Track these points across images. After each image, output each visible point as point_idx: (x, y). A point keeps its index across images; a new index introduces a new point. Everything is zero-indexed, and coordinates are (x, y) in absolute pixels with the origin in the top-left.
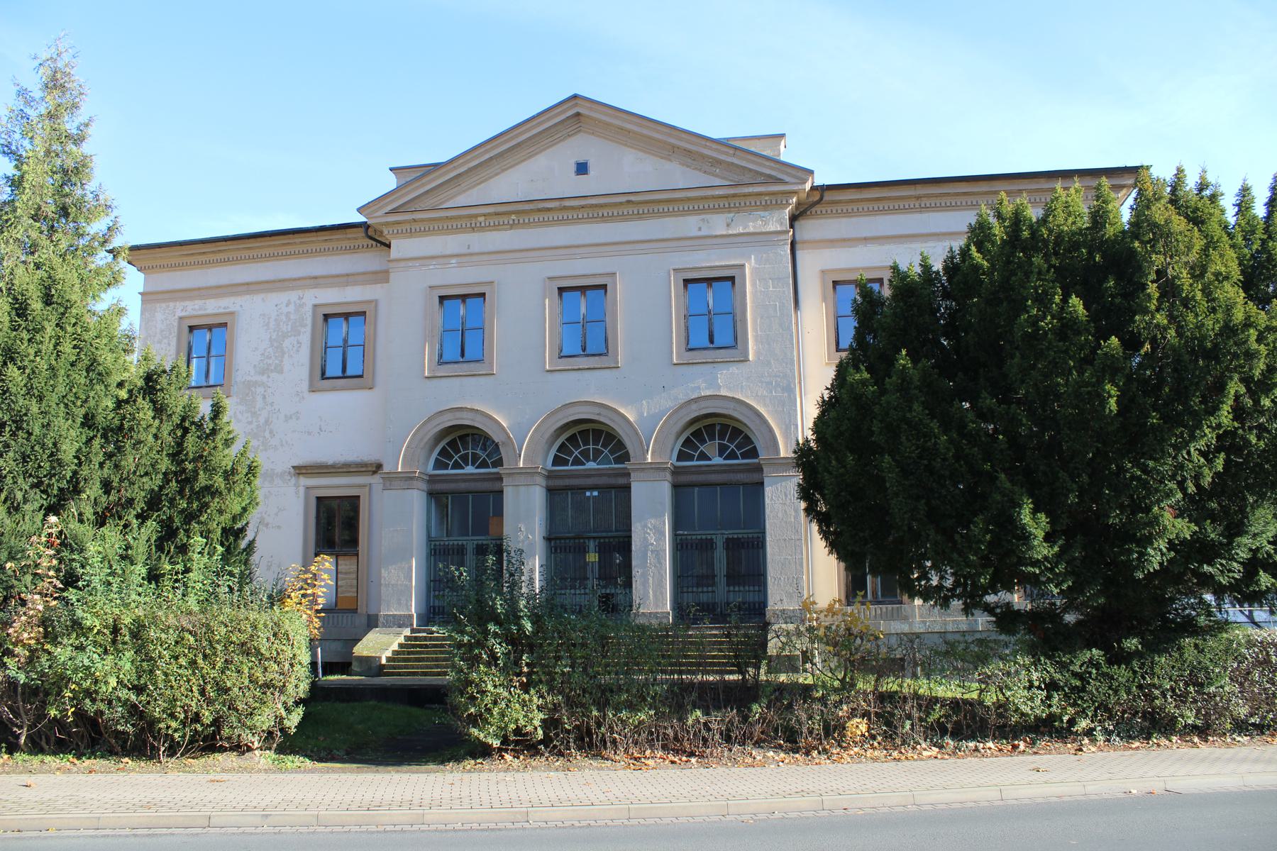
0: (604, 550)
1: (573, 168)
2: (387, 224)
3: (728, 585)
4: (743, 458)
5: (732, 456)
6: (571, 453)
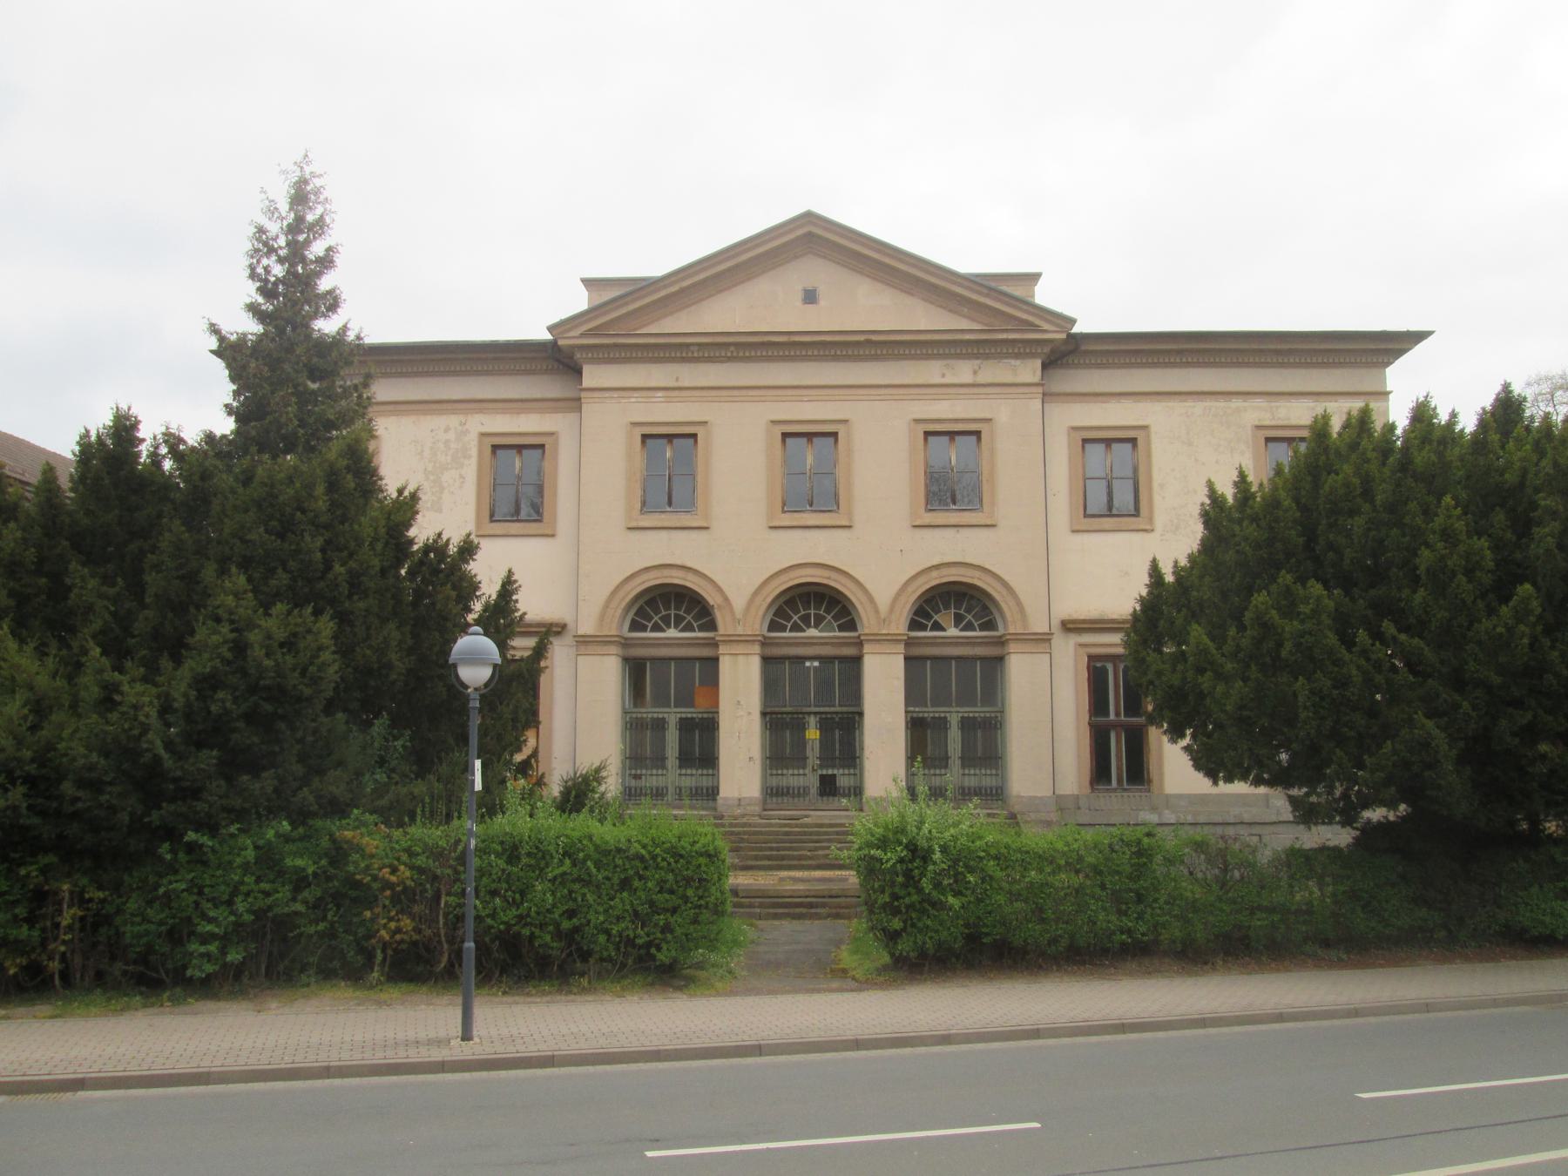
0: (826, 725)
1: (800, 296)
3: (963, 766)
4: (981, 629)
5: (969, 627)
6: (789, 618)
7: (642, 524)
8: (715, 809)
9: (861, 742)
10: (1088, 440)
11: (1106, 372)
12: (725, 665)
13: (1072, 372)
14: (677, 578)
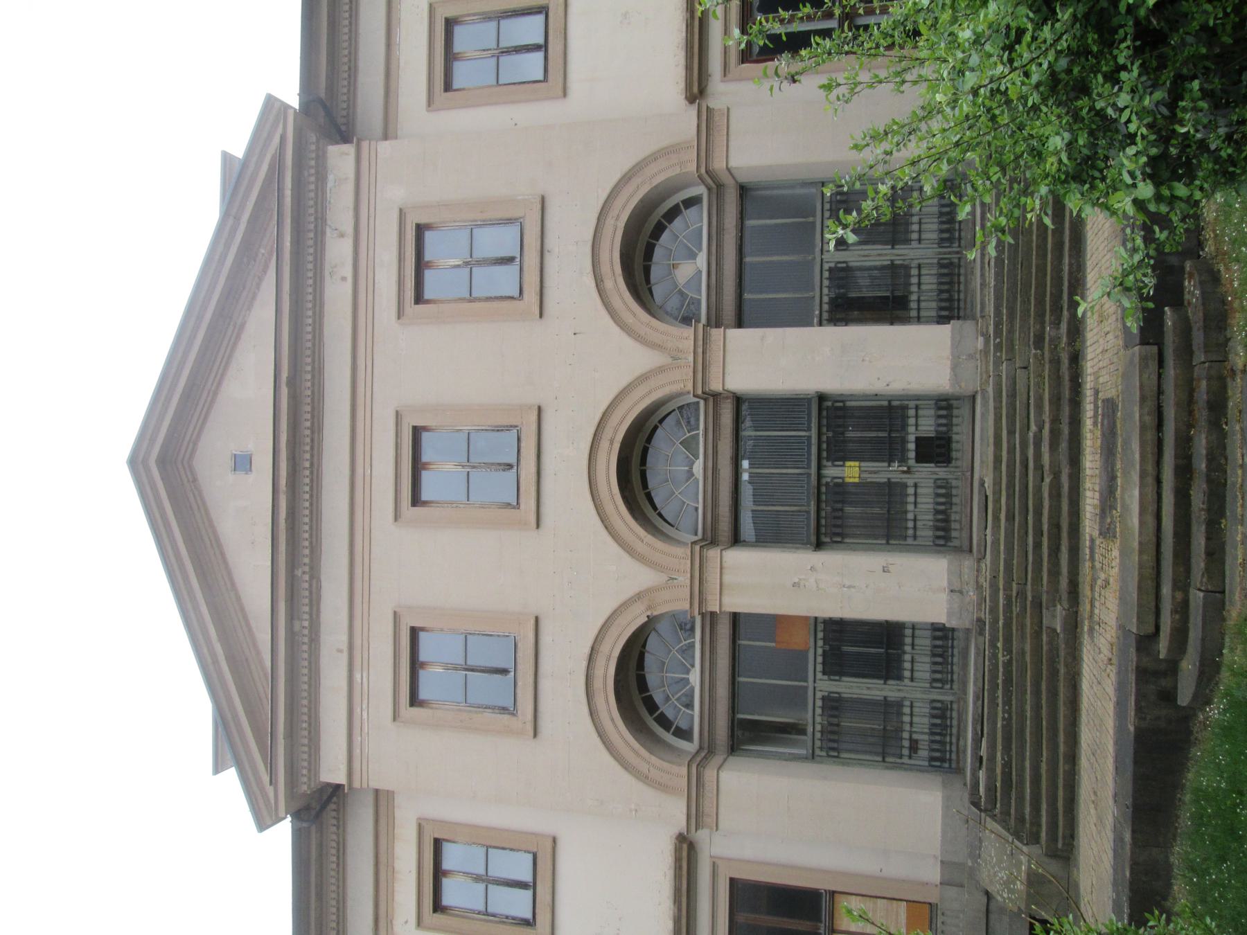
0: (837, 451)
2: (292, 782)
3: (907, 241)
7: (530, 716)
8: (968, 631)
9: (865, 397)
10: (446, 81)
11: (362, 65)
12: (737, 602)
13: (359, 110)
14: (607, 670)
